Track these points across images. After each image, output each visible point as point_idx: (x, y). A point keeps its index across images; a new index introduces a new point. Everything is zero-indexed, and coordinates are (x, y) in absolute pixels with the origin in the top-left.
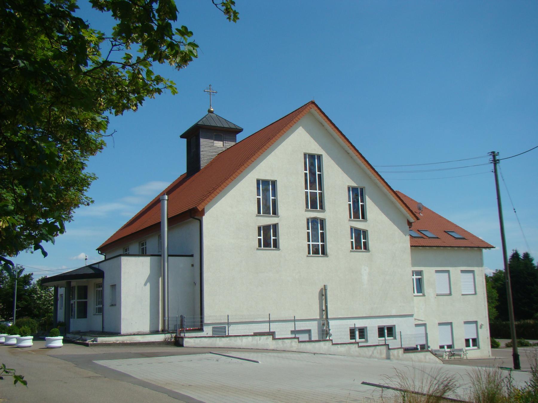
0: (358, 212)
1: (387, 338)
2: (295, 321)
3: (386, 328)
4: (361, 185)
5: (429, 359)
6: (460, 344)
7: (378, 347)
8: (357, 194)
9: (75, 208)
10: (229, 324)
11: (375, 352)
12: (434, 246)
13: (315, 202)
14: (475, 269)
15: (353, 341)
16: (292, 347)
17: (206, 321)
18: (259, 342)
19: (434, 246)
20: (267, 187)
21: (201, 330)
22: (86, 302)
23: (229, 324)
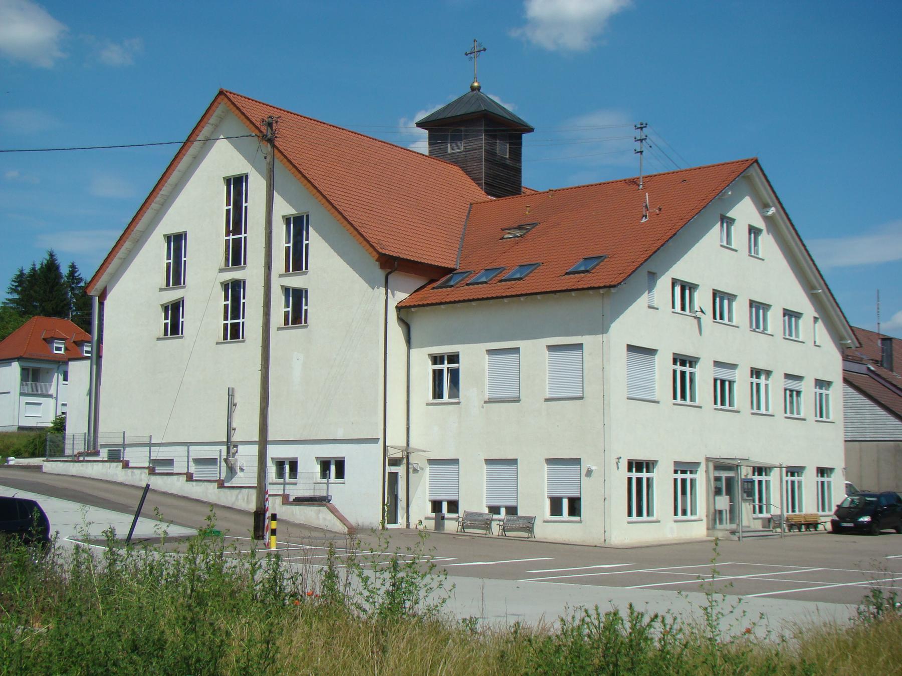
0: (297, 260)
1: (287, 479)
2: (150, 445)
3: (333, 462)
4: (303, 211)
5: (325, 519)
6: (534, 504)
7: (244, 490)
8: (298, 226)
9: (81, 280)
10: (124, 445)
11: (240, 497)
12: (474, 300)
13: (236, 255)
14: (586, 340)
15: (281, 481)
16: (141, 480)
17: (101, 441)
18: (109, 471)
19: (474, 300)
20: (177, 242)
21: (97, 453)
22: (448, 357)
23: (124, 445)
